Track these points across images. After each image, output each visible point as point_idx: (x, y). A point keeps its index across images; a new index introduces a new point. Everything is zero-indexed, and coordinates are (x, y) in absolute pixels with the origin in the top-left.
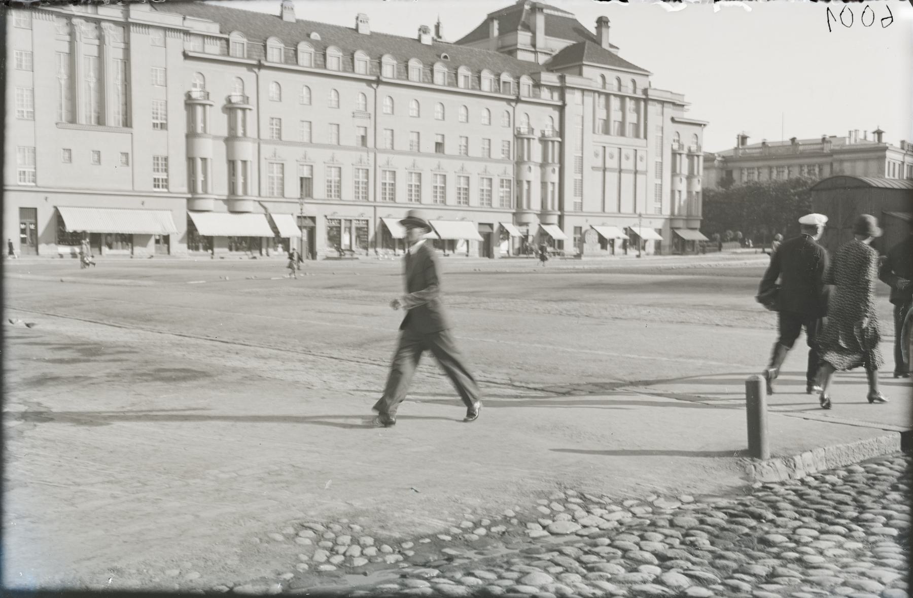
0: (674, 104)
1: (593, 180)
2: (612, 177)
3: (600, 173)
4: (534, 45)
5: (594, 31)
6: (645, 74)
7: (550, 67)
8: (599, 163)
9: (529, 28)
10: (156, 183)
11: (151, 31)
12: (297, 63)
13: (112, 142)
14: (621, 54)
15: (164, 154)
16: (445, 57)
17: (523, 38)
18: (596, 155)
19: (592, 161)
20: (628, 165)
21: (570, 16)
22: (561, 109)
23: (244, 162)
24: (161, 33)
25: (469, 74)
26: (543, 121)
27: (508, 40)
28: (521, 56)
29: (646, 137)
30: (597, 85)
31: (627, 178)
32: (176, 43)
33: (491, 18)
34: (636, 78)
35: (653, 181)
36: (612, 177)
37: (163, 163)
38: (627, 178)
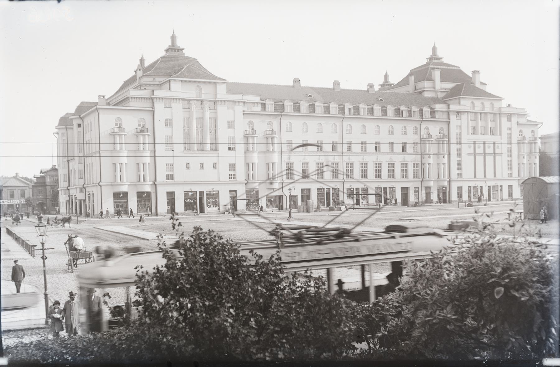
0: (518, 115)
1: (468, 161)
2: (480, 159)
3: (473, 157)
4: (434, 88)
5: (471, 76)
6: (499, 99)
7: (443, 101)
8: (472, 151)
9: (430, 79)
10: (231, 176)
11: (227, 103)
12: (329, 113)
13: (209, 160)
14: (488, 89)
15: (234, 162)
16: (381, 100)
17: (427, 84)
18: (470, 147)
19: (466, 149)
20: (489, 150)
21: (458, 68)
22: (449, 123)
23: (273, 163)
24: (232, 103)
25: (351, 107)
26: (418, 126)
27: (420, 85)
28: (426, 95)
29: (500, 135)
30: (468, 109)
31: (490, 159)
32: (239, 109)
33: (410, 74)
34: (493, 102)
35: (506, 158)
36: (480, 159)
37: (232, 167)
38: (490, 159)
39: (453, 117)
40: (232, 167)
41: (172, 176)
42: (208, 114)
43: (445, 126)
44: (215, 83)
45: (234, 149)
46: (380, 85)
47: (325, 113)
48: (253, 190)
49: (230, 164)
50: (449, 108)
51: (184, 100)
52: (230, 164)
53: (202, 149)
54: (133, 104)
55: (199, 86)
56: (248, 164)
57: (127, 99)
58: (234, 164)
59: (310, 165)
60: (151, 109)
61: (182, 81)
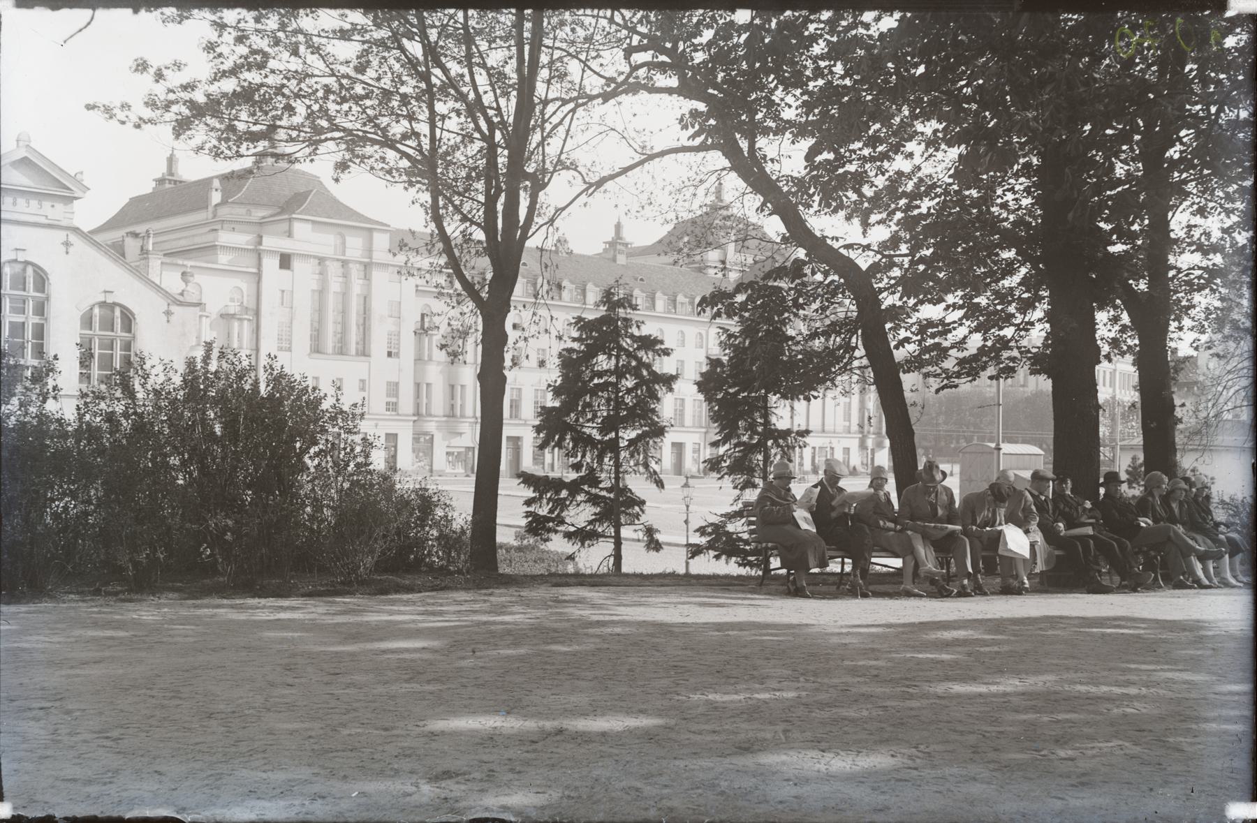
22: (259, 276)
23: (428, 385)
37: (393, 389)
39: (271, 264)
40: (393, 389)
41: (396, 404)
42: (357, 287)
43: (245, 285)
44: (370, 230)
45: (397, 355)
46: (155, 180)
47: (669, 312)
48: (426, 434)
49: (389, 383)
50: (260, 243)
51: (315, 257)
52: (389, 383)
53: (341, 351)
54: (224, 259)
55: (340, 234)
56: (452, 387)
57: (212, 248)
58: (397, 384)
59: (523, 392)
60: (254, 270)
61: (313, 222)
